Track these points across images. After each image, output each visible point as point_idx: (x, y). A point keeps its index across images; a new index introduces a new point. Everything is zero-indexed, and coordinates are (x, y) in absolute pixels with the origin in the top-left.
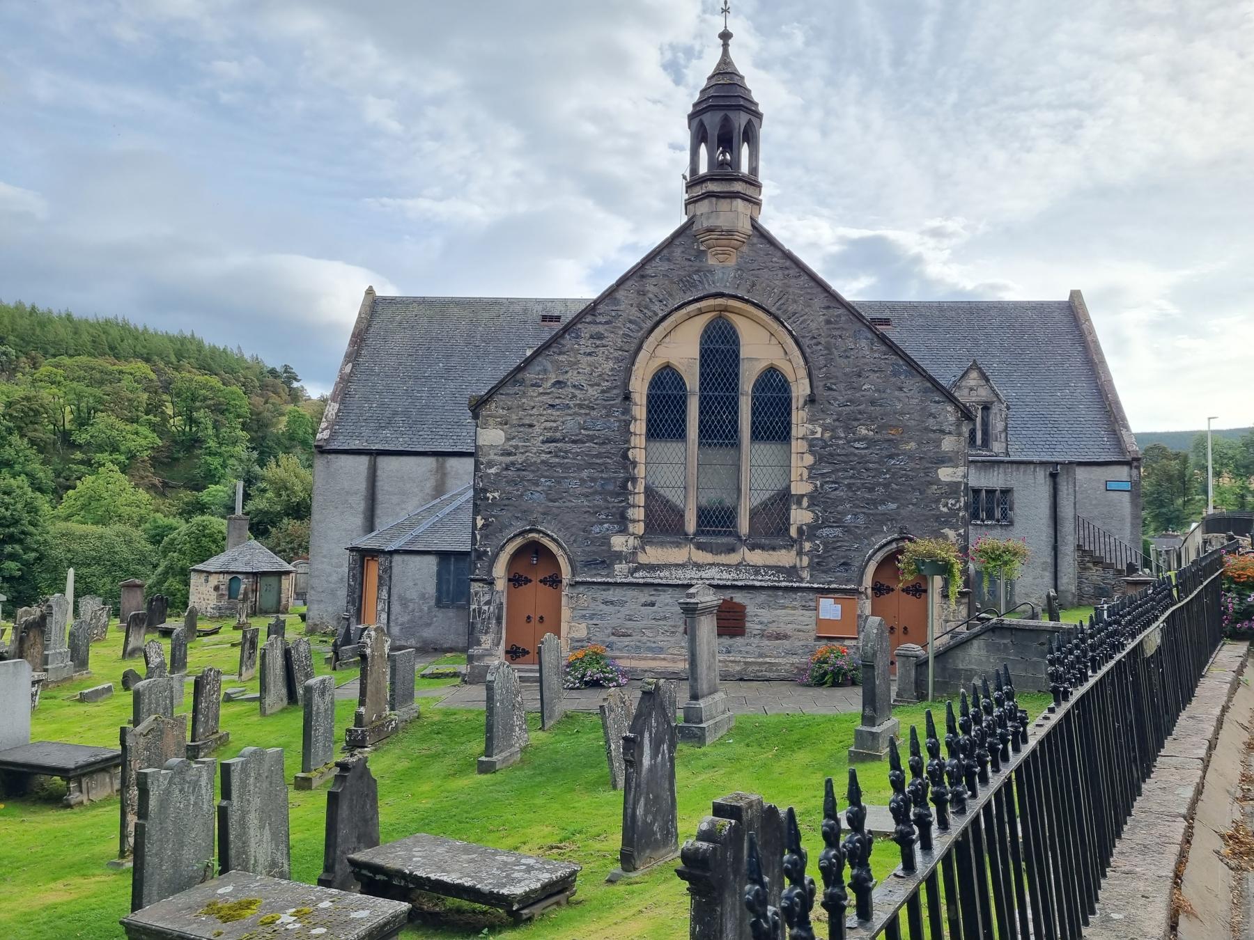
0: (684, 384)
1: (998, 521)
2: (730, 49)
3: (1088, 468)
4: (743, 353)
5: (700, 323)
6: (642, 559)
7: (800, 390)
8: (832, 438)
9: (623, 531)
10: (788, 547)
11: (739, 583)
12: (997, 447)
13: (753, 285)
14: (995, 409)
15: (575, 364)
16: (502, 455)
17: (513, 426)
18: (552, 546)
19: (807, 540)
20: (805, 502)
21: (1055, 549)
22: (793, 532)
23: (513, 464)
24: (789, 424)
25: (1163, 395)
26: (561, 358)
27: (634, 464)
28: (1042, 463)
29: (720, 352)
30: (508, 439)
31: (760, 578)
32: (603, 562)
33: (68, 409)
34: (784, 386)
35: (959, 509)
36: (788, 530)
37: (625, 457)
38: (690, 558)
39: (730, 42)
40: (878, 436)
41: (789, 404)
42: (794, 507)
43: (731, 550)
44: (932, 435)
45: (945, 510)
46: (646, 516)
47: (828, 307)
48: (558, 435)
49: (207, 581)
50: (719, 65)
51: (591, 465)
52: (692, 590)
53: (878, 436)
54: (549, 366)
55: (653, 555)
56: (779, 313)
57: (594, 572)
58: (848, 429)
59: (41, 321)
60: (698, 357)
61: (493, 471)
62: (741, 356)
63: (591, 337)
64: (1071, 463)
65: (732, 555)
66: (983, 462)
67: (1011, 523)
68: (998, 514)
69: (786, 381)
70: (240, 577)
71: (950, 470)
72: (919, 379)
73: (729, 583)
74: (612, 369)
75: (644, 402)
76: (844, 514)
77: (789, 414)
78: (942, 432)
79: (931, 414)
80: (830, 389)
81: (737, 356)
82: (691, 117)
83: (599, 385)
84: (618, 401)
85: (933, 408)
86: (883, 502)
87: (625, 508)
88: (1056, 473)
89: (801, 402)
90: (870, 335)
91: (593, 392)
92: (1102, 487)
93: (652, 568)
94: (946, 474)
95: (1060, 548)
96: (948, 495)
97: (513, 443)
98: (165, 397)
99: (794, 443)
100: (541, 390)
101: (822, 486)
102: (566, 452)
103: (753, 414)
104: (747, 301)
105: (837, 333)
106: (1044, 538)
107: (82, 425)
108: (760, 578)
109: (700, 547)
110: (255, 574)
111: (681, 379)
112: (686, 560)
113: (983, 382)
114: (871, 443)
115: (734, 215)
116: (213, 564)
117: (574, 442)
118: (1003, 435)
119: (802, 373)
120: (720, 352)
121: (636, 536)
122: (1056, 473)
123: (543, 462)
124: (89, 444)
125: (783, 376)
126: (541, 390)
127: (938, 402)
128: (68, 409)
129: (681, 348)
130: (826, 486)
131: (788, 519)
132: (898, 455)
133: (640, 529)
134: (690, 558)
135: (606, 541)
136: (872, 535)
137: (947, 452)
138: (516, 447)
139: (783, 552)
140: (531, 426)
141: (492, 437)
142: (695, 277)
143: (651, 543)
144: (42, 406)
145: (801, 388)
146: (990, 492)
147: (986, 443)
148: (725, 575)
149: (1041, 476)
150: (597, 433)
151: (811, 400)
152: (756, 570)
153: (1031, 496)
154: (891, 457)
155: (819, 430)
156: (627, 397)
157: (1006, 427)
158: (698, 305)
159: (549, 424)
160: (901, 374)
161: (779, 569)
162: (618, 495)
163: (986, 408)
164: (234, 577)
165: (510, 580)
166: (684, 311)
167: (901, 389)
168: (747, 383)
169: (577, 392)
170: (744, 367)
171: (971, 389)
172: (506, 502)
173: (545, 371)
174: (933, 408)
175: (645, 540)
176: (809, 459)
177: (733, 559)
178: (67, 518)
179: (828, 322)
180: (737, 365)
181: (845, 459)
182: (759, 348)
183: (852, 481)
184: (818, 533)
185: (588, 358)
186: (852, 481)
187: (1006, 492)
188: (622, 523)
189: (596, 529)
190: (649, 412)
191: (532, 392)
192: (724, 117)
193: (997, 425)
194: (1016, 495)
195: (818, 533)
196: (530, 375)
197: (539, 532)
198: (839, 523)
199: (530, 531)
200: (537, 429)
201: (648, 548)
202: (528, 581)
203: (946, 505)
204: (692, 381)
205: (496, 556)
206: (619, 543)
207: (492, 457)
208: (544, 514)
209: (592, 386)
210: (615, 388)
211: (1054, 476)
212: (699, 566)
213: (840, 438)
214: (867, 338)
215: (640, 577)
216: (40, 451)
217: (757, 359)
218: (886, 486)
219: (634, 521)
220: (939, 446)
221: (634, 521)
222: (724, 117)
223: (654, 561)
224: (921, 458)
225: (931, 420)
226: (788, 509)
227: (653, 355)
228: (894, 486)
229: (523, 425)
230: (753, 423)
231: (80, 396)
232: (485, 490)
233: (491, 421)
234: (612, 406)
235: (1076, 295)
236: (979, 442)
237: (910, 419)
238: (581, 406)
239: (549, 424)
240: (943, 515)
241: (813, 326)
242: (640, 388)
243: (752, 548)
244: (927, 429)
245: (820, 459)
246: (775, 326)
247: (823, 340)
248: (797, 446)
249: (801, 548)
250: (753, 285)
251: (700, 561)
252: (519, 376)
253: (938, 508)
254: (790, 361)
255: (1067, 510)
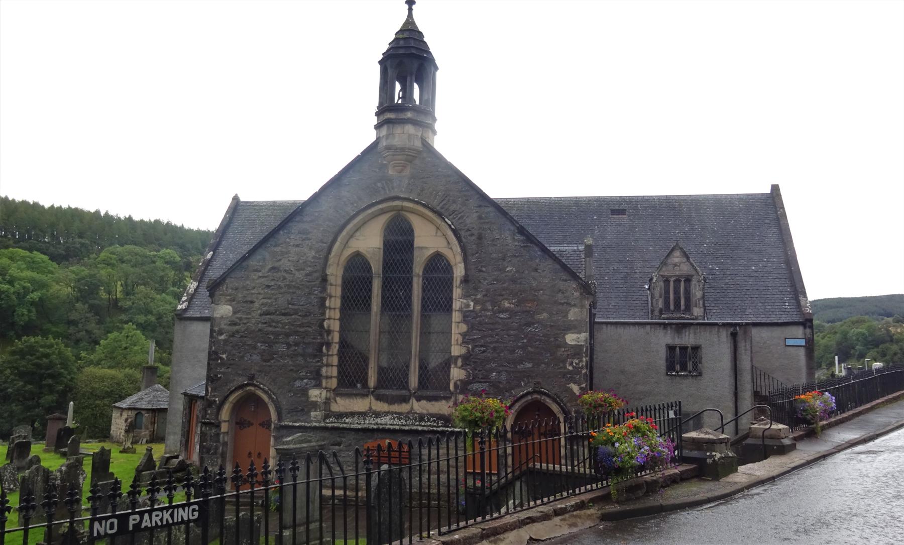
0: (371, 268)
1: (690, 372)
2: (414, 12)
3: (771, 328)
4: (417, 243)
5: (383, 220)
6: (335, 408)
7: (459, 271)
8: (481, 310)
9: (318, 385)
10: (447, 398)
11: (406, 428)
12: (697, 311)
13: (422, 190)
14: (694, 282)
15: (287, 253)
16: (230, 325)
17: (239, 302)
18: (265, 397)
19: (461, 393)
20: (460, 363)
21: (736, 394)
22: (452, 387)
23: (237, 332)
24: (451, 299)
25: (833, 269)
26: (278, 249)
27: (329, 332)
28: (724, 325)
29: (399, 243)
30: (235, 313)
31: (423, 424)
32: (302, 410)
33: (119, 283)
34: (448, 268)
35: (582, 368)
36: (448, 384)
37: (322, 326)
38: (370, 408)
39: (414, 7)
40: (519, 309)
41: (452, 284)
42: (453, 366)
43: (404, 400)
44: (560, 307)
45: (571, 368)
46: (339, 372)
47: (480, 206)
48: (272, 309)
49: (121, 415)
50: (405, 24)
51: (296, 333)
52: (657, 407)
53: (519, 309)
54: (267, 256)
55: (342, 405)
56: (443, 211)
57: (295, 418)
58: (494, 303)
59: (109, 220)
60: (382, 247)
61: (222, 337)
62: (416, 245)
63: (300, 233)
64: (747, 324)
65: (404, 405)
66: (677, 324)
67: (700, 374)
68: (690, 366)
69: (449, 264)
70: (143, 412)
71: (575, 336)
72: (550, 262)
73: (397, 427)
74: (314, 257)
75: (339, 281)
76: (492, 370)
77: (452, 291)
78: (568, 304)
79: (560, 291)
80: (481, 271)
81: (412, 245)
82: (381, 62)
83: (304, 270)
84: (318, 282)
85: (562, 285)
86: (521, 362)
87: (321, 367)
88: (736, 332)
89: (458, 282)
90: (512, 228)
91: (299, 275)
92: (782, 343)
93: (340, 416)
94: (571, 339)
95: (740, 394)
96: (574, 356)
97: (238, 315)
98: (186, 273)
99: (454, 314)
100: (260, 274)
101: (473, 349)
102: (277, 322)
103: (424, 290)
104: (417, 203)
105: (486, 226)
106: (727, 385)
107: (128, 294)
108: (423, 424)
109: (379, 398)
110: (153, 410)
111: (369, 264)
112: (367, 408)
113: (685, 260)
114: (512, 313)
115: (404, 135)
116: (124, 404)
117: (284, 314)
118: (701, 302)
119: (459, 258)
120: (399, 243)
121: (328, 389)
122: (736, 332)
123: (260, 330)
124: (130, 308)
125: (447, 261)
126: (260, 274)
127: (566, 280)
128: (119, 283)
129: (370, 241)
130: (477, 349)
131: (449, 375)
132: (534, 324)
133: (334, 383)
134: (370, 408)
135: (304, 392)
136: (513, 389)
137: (572, 321)
138: (240, 319)
139: (444, 402)
140: (252, 302)
141: (224, 310)
142: (379, 184)
143: (342, 395)
144: (99, 281)
145: (459, 271)
146: (684, 349)
147: (688, 308)
148: (396, 421)
149: (725, 335)
150: (301, 308)
151: (466, 280)
152: (421, 418)
153: (716, 352)
154: (529, 324)
155: (472, 304)
156: (324, 279)
157: (704, 295)
158: (380, 206)
159: (265, 301)
160: (536, 258)
161: (440, 417)
162: (315, 356)
163: (688, 280)
164: (139, 411)
165: (237, 423)
166: (370, 211)
167: (536, 270)
168: (418, 269)
169: (287, 276)
170: (416, 253)
171: (675, 265)
172: (232, 362)
173: (264, 259)
174: (562, 285)
175: (337, 392)
176: (464, 328)
177: (404, 408)
178: (98, 363)
179: (480, 218)
180: (412, 253)
181: (492, 327)
182: (429, 239)
183: (497, 345)
184: (469, 387)
185: (297, 249)
186: (497, 345)
187: (696, 348)
188: (317, 379)
189: (298, 384)
190: (343, 290)
191: (254, 276)
192: (408, 59)
193: (697, 293)
194: (703, 350)
195: (469, 387)
196: (253, 262)
197: (255, 386)
198: (486, 379)
199: (248, 385)
200: (256, 305)
201: (338, 399)
202: (250, 424)
203: (571, 364)
204: (376, 267)
205: (222, 403)
206: (315, 394)
207: (223, 326)
208: (260, 371)
209: (298, 270)
210: (316, 272)
211: (734, 335)
212: (378, 415)
213: (487, 310)
214: (509, 230)
215: (331, 423)
216: (97, 314)
217: (426, 248)
218: (523, 347)
219: (327, 377)
220: (566, 316)
221: (327, 377)
222: (408, 59)
223: (342, 409)
224: (551, 326)
225: (560, 295)
226: (449, 368)
227: (345, 245)
228: (530, 348)
229: (246, 302)
230: (423, 298)
231: (127, 276)
232: (216, 353)
233: (223, 299)
234: (314, 286)
235: (775, 188)
236: (683, 307)
237: (543, 294)
238: (289, 287)
239: (265, 301)
240: (570, 372)
241: (468, 221)
242: (335, 273)
243: (419, 399)
244: (556, 303)
245: (471, 328)
246: (438, 221)
247: (476, 232)
248: (456, 316)
249: (456, 400)
250: (422, 190)
251: (378, 410)
252: (244, 264)
253: (565, 367)
254: (451, 248)
255: (745, 363)
